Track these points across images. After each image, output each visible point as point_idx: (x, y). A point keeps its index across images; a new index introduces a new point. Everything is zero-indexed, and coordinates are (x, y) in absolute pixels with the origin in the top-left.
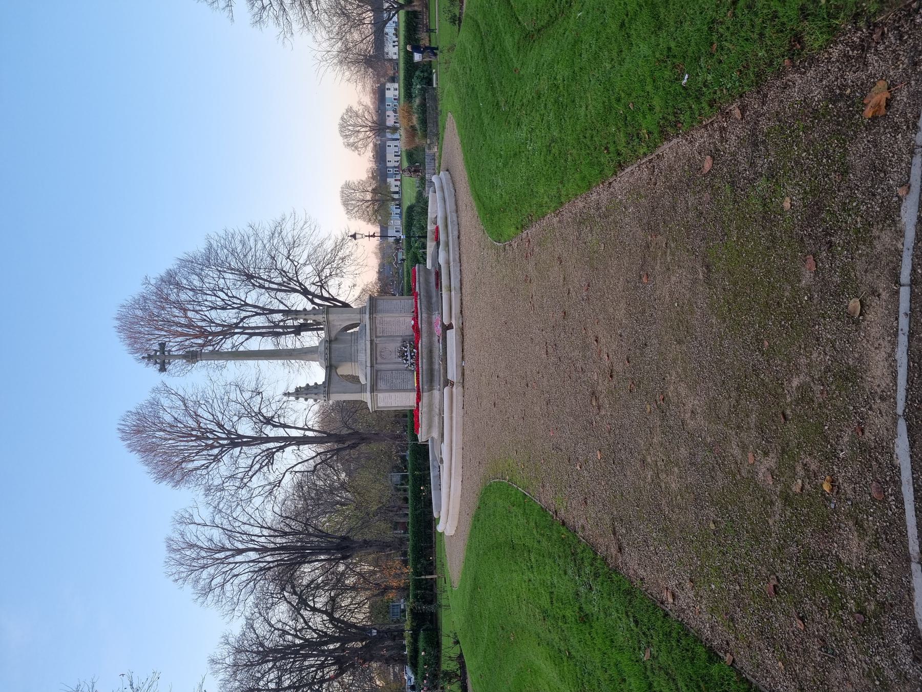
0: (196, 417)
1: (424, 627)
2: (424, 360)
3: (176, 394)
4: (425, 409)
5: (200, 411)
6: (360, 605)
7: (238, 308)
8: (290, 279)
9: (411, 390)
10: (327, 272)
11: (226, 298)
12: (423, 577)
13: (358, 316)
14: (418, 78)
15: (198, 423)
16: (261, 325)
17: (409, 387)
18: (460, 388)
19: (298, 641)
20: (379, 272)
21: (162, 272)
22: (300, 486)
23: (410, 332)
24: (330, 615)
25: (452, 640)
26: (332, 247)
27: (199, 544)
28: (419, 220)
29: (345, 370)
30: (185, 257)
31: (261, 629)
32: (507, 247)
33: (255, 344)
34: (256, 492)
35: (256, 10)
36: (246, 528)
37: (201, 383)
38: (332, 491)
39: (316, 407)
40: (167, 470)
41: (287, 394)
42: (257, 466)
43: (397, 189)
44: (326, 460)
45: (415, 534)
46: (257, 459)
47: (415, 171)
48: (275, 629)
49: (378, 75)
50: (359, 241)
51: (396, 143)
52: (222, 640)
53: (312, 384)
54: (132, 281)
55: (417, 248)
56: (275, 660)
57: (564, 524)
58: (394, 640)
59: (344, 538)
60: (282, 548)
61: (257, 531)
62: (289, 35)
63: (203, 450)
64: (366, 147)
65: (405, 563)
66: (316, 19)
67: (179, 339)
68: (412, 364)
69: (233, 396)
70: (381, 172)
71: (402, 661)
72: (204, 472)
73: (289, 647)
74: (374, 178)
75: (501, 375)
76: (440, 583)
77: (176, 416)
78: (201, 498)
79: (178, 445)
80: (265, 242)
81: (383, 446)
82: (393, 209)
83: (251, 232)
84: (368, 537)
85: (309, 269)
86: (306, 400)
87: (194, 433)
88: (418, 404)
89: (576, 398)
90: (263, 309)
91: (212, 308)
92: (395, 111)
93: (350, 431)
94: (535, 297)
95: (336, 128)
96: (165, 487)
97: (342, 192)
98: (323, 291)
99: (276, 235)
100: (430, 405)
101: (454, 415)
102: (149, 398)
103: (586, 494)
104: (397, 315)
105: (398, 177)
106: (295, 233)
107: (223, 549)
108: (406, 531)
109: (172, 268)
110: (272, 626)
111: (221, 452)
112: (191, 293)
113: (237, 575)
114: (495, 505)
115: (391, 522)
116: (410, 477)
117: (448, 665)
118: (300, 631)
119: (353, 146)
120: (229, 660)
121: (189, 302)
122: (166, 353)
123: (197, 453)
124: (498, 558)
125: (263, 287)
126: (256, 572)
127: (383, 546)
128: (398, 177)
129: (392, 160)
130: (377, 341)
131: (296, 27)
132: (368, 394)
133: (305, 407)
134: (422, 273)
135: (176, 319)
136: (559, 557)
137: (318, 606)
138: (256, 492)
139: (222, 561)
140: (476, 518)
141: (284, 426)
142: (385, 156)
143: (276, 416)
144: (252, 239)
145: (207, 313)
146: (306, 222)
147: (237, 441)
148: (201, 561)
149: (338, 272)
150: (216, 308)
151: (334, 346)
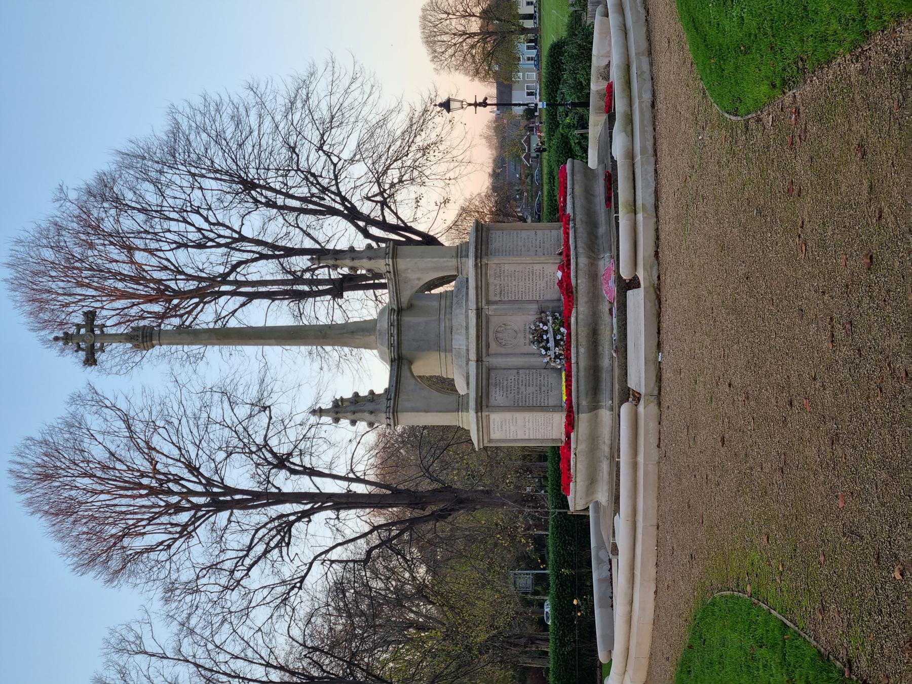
2: (582, 350)
3: (113, 407)
4: (582, 447)
5: (156, 441)
7: (226, 245)
8: (324, 190)
9: (556, 408)
10: (393, 175)
11: (206, 226)
13: (453, 262)
15: (153, 462)
18: (653, 407)
20: (495, 175)
22: (339, 589)
23: (553, 293)
28: (574, 72)
29: (427, 366)
33: (259, 314)
34: (258, 597)
37: (158, 388)
38: (400, 600)
39: (371, 438)
40: (95, 550)
42: (259, 549)
43: (530, 10)
44: (389, 540)
53: (363, 393)
55: (569, 126)
63: (161, 514)
69: (216, 414)
72: (163, 556)
75: (737, 382)
77: (113, 449)
78: (157, 606)
79: (127, 504)
80: (278, 118)
81: (499, 516)
83: (251, 99)
85: (359, 170)
86: (353, 423)
87: (145, 481)
88: (568, 436)
89: (892, 433)
90: (273, 247)
91: (180, 245)
93: (436, 485)
94: (808, 226)
97: (424, 18)
99: (299, 104)
100: (593, 438)
101: (641, 459)
102: (64, 413)
104: (528, 259)
106: (334, 99)
109: (105, 168)
111: (194, 520)
114: (723, 642)
115: (515, 667)
116: (552, 579)
121: (137, 234)
122: (97, 332)
130: (489, 310)
133: (351, 435)
134: (578, 177)
135: (114, 267)
138: (258, 597)
141: (312, 472)
144: (253, 114)
145: (169, 255)
146: (354, 79)
147: (223, 499)
149: (414, 175)
150: (186, 246)
151: (407, 319)
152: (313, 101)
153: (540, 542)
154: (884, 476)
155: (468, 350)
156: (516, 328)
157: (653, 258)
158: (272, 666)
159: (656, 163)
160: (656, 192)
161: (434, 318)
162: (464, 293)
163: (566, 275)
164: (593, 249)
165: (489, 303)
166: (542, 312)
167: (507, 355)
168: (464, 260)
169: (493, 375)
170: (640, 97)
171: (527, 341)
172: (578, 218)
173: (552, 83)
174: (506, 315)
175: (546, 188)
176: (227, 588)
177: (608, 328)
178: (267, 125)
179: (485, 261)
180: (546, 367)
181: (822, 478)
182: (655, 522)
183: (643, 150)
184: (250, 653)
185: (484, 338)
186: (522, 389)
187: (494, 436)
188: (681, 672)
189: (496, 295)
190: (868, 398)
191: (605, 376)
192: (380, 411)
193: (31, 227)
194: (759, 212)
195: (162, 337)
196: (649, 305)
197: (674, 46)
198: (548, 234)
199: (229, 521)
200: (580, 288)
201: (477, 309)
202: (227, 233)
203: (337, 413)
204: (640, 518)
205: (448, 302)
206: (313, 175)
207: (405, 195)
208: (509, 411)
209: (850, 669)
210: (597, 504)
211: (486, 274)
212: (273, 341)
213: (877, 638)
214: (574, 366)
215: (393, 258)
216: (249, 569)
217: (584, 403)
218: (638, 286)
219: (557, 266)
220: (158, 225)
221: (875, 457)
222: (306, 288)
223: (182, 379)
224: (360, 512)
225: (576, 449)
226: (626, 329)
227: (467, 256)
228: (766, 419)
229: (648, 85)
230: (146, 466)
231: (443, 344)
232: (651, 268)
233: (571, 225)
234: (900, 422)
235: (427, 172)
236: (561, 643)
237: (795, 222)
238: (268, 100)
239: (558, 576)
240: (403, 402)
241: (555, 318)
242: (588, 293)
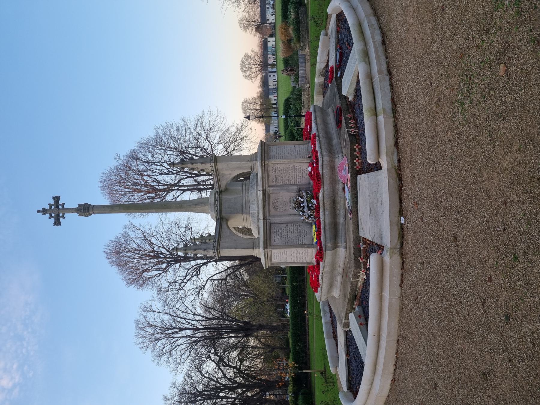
0: (151, 243)
2: (327, 213)
4: (327, 269)
7: (176, 174)
9: (311, 246)
13: (249, 164)
17: (307, 243)
23: (306, 179)
26: (235, 131)
27: (155, 324)
28: (295, 105)
29: (236, 222)
30: (142, 141)
33: (187, 196)
36: (182, 315)
43: (275, 102)
47: (291, 70)
48: (205, 377)
55: (293, 126)
64: (256, 77)
67: (140, 194)
68: (309, 216)
69: (174, 231)
70: (266, 91)
79: (139, 262)
80: (192, 129)
83: (182, 123)
84: (262, 323)
91: (161, 174)
95: (239, 67)
96: (133, 288)
97: (243, 105)
99: (199, 125)
100: (333, 265)
102: (122, 232)
104: (292, 161)
105: (276, 95)
109: (133, 148)
110: (203, 375)
111: (168, 266)
112: (146, 164)
119: (249, 77)
122: (60, 207)
128: (276, 95)
130: (270, 190)
142: (268, 82)
144: (184, 129)
145: (156, 177)
146: (218, 116)
148: (157, 335)
151: (225, 197)
155: (258, 213)
156: (285, 200)
157: (393, 148)
158: (196, 315)
159: (391, 79)
160: (393, 99)
161: (239, 196)
162: (255, 181)
165: (269, 186)
166: (300, 191)
167: (280, 216)
168: (254, 162)
169: (273, 227)
170: (373, 38)
171: (292, 208)
172: (321, 135)
174: (279, 193)
177: (342, 199)
178: (188, 133)
179: (267, 162)
180: (303, 222)
182: (396, 338)
183: (380, 72)
185: (267, 206)
186: (290, 235)
187: (273, 261)
189: (273, 182)
191: (341, 228)
192: (209, 249)
193: (108, 169)
195: (94, 209)
196: (392, 182)
198: (302, 147)
200: (325, 175)
201: (263, 190)
203: (185, 250)
205: (247, 187)
206: (205, 149)
208: (283, 248)
211: (268, 170)
212: (154, 210)
215: (214, 162)
216: (186, 283)
217: (329, 245)
219: (308, 164)
222: (202, 187)
225: (323, 270)
226: (357, 199)
227: (257, 160)
229: (378, 31)
231: (244, 210)
232: (392, 154)
233: (317, 139)
235: (243, 146)
240: (222, 244)
242: (330, 178)
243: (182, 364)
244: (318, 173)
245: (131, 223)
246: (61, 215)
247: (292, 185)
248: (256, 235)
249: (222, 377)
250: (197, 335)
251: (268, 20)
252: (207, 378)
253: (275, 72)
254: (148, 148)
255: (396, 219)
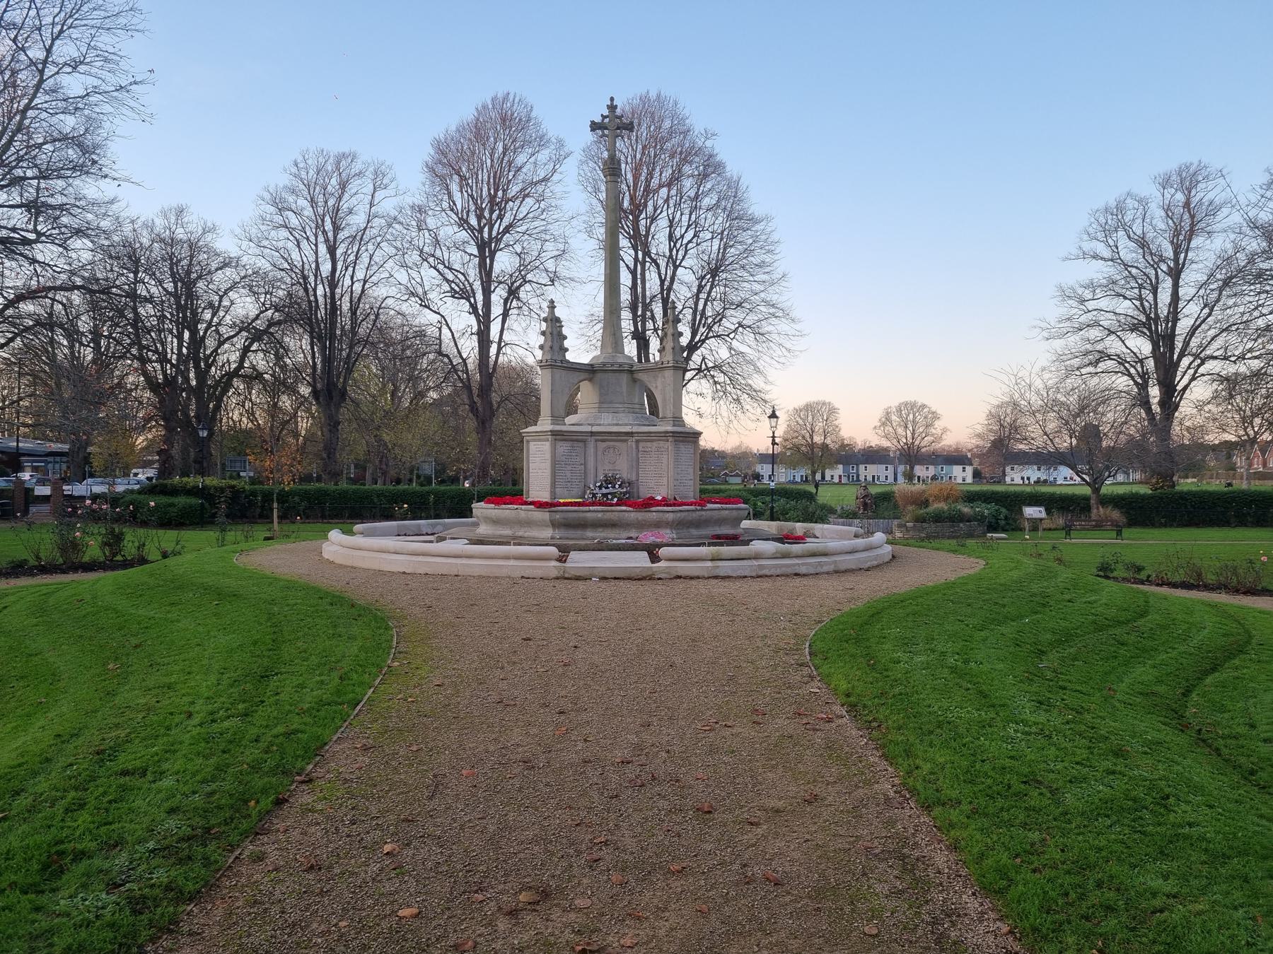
1: (207, 505)
2: (600, 515)
3: (554, 171)
4: (523, 514)
5: (529, 201)
6: (251, 414)
7: (671, 256)
8: (710, 328)
9: (553, 493)
10: (720, 378)
11: (685, 241)
12: (275, 505)
13: (669, 415)
14: (994, 512)
15: (512, 199)
16: (648, 285)
18: (554, 573)
19: (201, 327)
20: (713, 451)
21: (721, 157)
22: (421, 334)
23: (645, 493)
24: (235, 373)
25: (169, 550)
26: (754, 386)
27: (346, 197)
29: (586, 395)
30: (743, 186)
31: (222, 278)
32: (806, 671)
34: (414, 274)
35: (1080, 291)
36: (365, 259)
37: (568, 211)
38: (413, 379)
39: (531, 360)
40: (450, 156)
41: (552, 306)
42: (451, 277)
43: (828, 478)
44: (456, 371)
45: (343, 495)
46: (460, 276)
47: (865, 505)
48: (221, 297)
49: (983, 456)
50: (766, 422)
51: (891, 479)
52: (209, 224)
53: (566, 343)
54: (711, 118)
55: (755, 505)
56: (176, 295)
57: (280, 802)
58: (195, 462)
59: (343, 394)
60: (333, 309)
61: (360, 275)
62: (1045, 334)
63: (476, 204)
65: (307, 478)
66: (1069, 372)
68: (594, 495)
69: (549, 246)
70: (850, 457)
71: (164, 472)
72: (445, 205)
73: (194, 313)
74: (843, 446)
75: (579, 655)
76: (260, 531)
77: (524, 170)
78: (409, 200)
79: (484, 172)
80: (762, 295)
81: (473, 451)
82: (800, 473)
83: (776, 276)
85: (724, 353)
86: (541, 347)
87: (500, 193)
88: (532, 503)
89: (535, 841)
90: (670, 289)
91: (671, 222)
92: (934, 478)
93: (495, 405)
94: (727, 732)
96: (427, 152)
97: (824, 404)
98: (694, 373)
99: (772, 310)
100: (529, 523)
101: (512, 562)
102: (550, 134)
103: (330, 867)
105: (844, 480)
106: (775, 336)
107: (337, 228)
108: (353, 481)
109: (728, 169)
110: (226, 293)
113: (299, 246)
114: (352, 638)
115: (366, 461)
116: (427, 488)
117: (132, 538)
118: (217, 331)
119: (886, 420)
120: (180, 234)
121: (680, 191)
123: (472, 196)
124: (255, 643)
125: (699, 291)
126: (302, 272)
127: (330, 449)
128: (844, 480)
129: (868, 471)
130: (631, 442)
131: (1058, 344)
132: (550, 428)
133: (532, 344)
134: (735, 513)
135: (657, 174)
136: (212, 793)
137: (251, 356)
138: (414, 274)
139: (319, 226)
140: (337, 600)
141: (505, 315)
143: (520, 304)
144: (765, 277)
145: (665, 214)
146: (789, 351)
147: (487, 250)
148: (321, 199)
149: (720, 392)
150: (671, 226)
151: (624, 378)
152: (773, 320)
153: (455, 480)
154: (491, 828)
160: (729, 577)
163: (658, 503)
164: (679, 525)
165: (637, 441)
169: (581, 444)
170: (803, 564)
173: (782, 492)
175: (710, 487)
176: (421, 251)
178: (757, 287)
180: (586, 487)
181: (492, 748)
184: (375, 268)
187: (532, 444)
188: (334, 596)
190: (570, 808)
191: (579, 533)
193: (686, 112)
194: (731, 679)
197: (849, 594)
198: (690, 490)
199: (471, 255)
202: (680, 257)
204: (464, 561)
207: (702, 385)
209: (303, 782)
210: (476, 525)
213: (328, 818)
214: (587, 508)
218: (653, 562)
220: (686, 207)
221: (511, 816)
223: (574, 222)
224: (476, 350)
228: (547, 685)
229: (812, 571)
230: (511, 194)
234: (546, 851)
235: (722, 402)
236: (380, 494)
237: (728, 718)
238: (776, 287)
239: (428, 493)
240: (559, 373)
241: (625, 494)
243: (258, 251)
244: (652, 505)
245: (568, 155)
246: (606, 132)
247: (638, 474)
248: (570, 419)
249: (220, 335)
250: (320, 288)
251: (1012, 469)
252: (220, 301)
253: (896, 479)
254: (726, 198)
255: (596, 572)
